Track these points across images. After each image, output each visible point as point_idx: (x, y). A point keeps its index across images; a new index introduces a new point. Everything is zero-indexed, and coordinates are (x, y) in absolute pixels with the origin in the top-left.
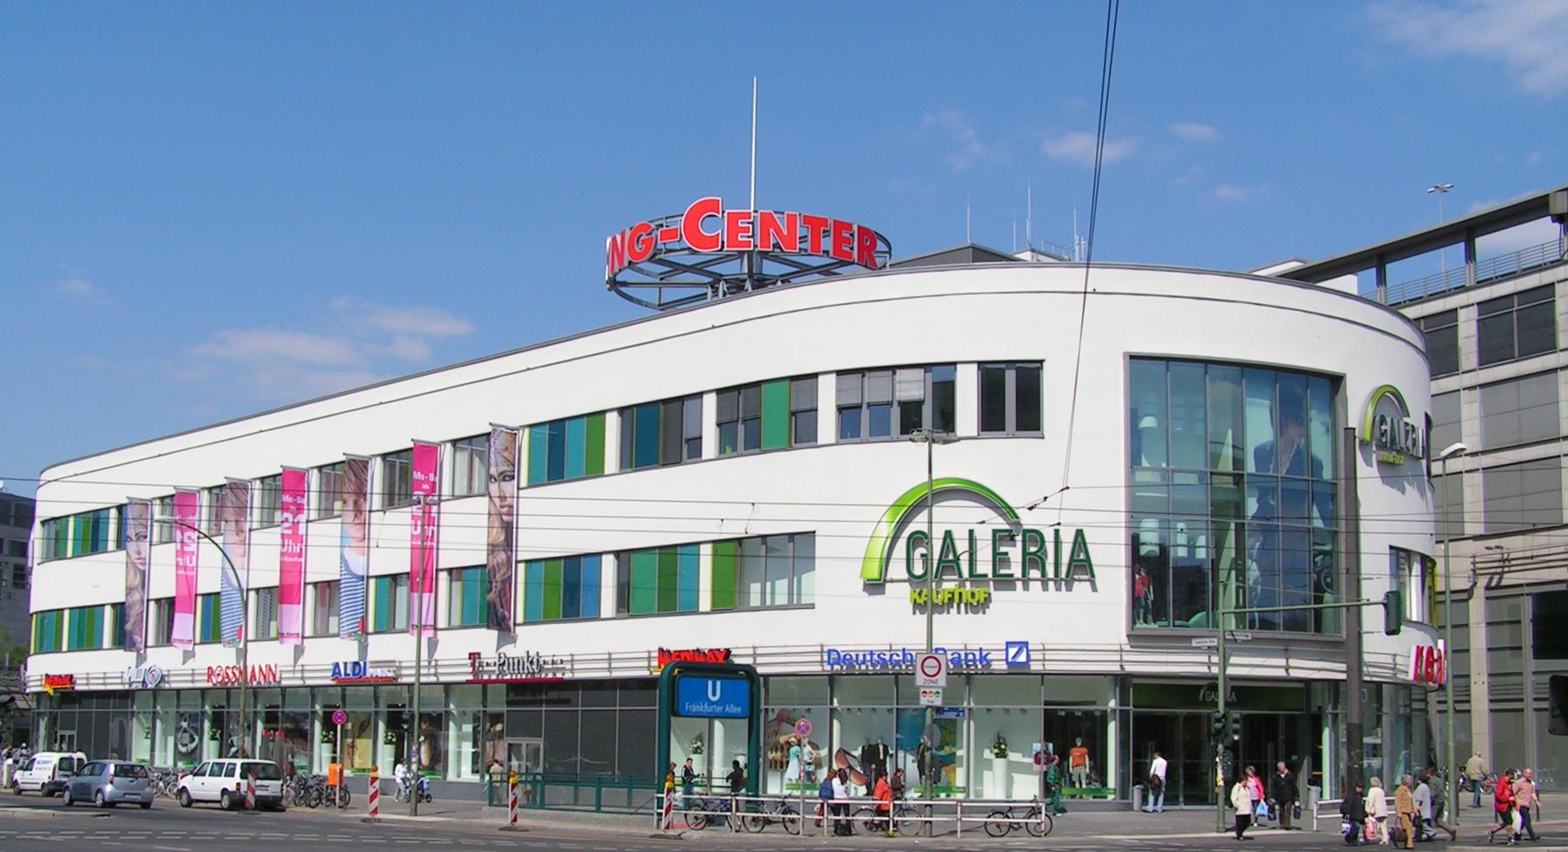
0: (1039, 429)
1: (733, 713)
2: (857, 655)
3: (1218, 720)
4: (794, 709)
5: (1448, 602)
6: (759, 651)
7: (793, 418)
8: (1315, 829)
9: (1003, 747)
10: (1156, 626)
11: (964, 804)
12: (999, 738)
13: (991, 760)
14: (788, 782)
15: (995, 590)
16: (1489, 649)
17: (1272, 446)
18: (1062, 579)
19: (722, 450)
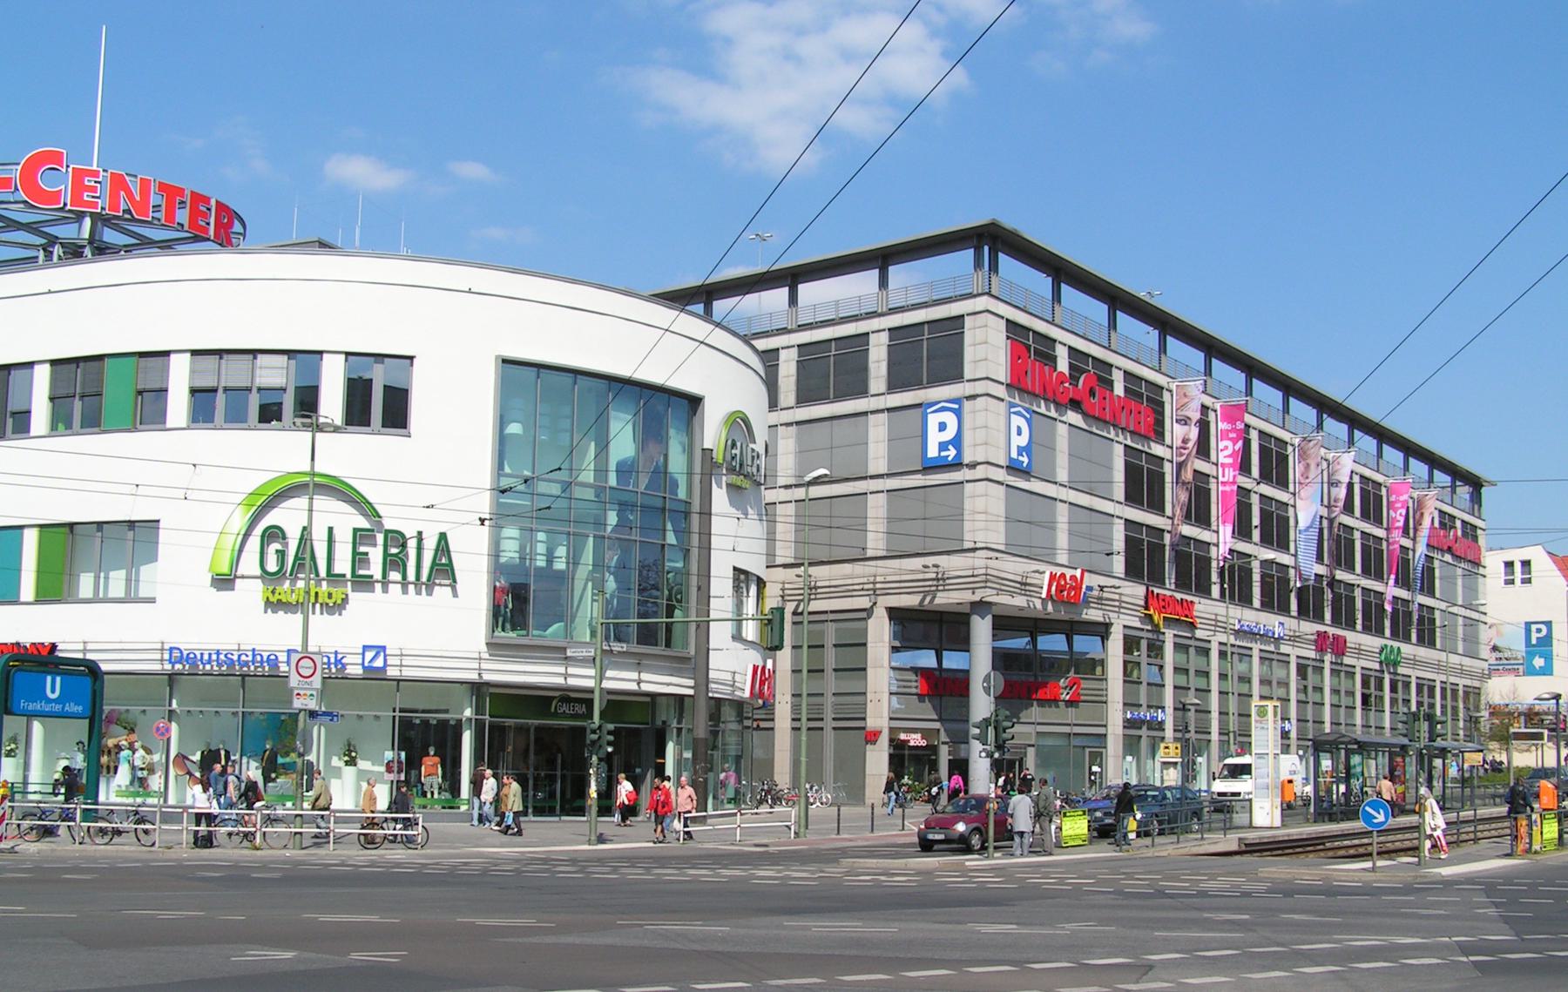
0: (405, 428)
1: (73, 713)
2: (202, 654)
3: (594, 732)
4: (128, 710)
5: (806, 623)
6: (89, 647)
7: (140, 397)
8: (738, 838)
9: (353, 754)
10: (515, 635)
11: (338, 815)
12: (349, 745)
13: (340, 768)
14: (117, 788)
15: (353, 591)
16: (793, 671)
17: (633, 462)
18: (423, 584)
19: (54, 427)
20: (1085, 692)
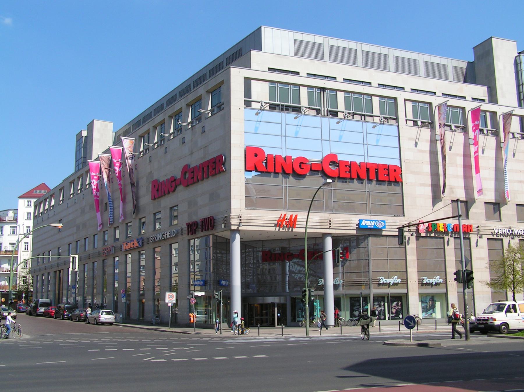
20: (245, 221)
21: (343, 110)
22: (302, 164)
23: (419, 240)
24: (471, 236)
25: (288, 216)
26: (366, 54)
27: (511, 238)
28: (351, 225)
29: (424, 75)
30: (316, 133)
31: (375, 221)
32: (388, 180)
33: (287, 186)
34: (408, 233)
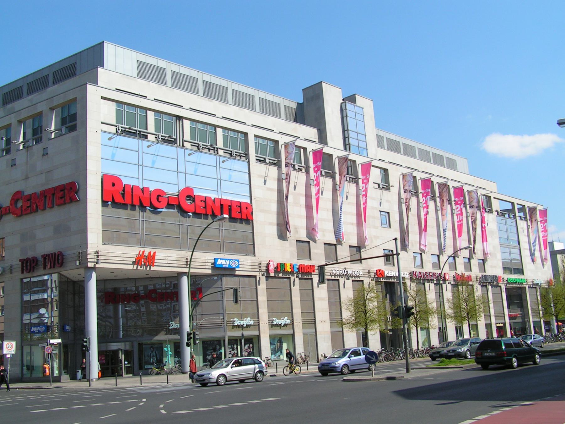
21: (153, 132)
22: (159, 197)
23: (268, 280)
24: (313, 276)
25: (146, 253)
26: (206, 84)
27: (346, 279)
28: (207, 264)
29: (259, 110)
30: (172, 165)
31: (230, 260)
32: (205, 213)
33: (144, 220)
34: (259, 273)
